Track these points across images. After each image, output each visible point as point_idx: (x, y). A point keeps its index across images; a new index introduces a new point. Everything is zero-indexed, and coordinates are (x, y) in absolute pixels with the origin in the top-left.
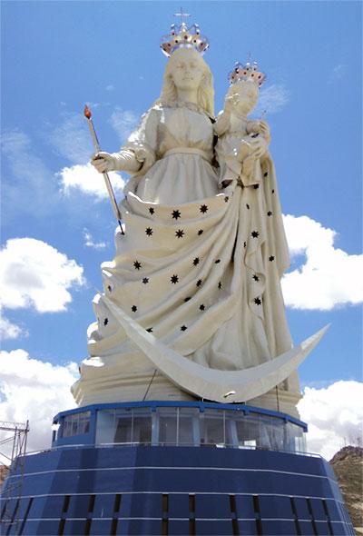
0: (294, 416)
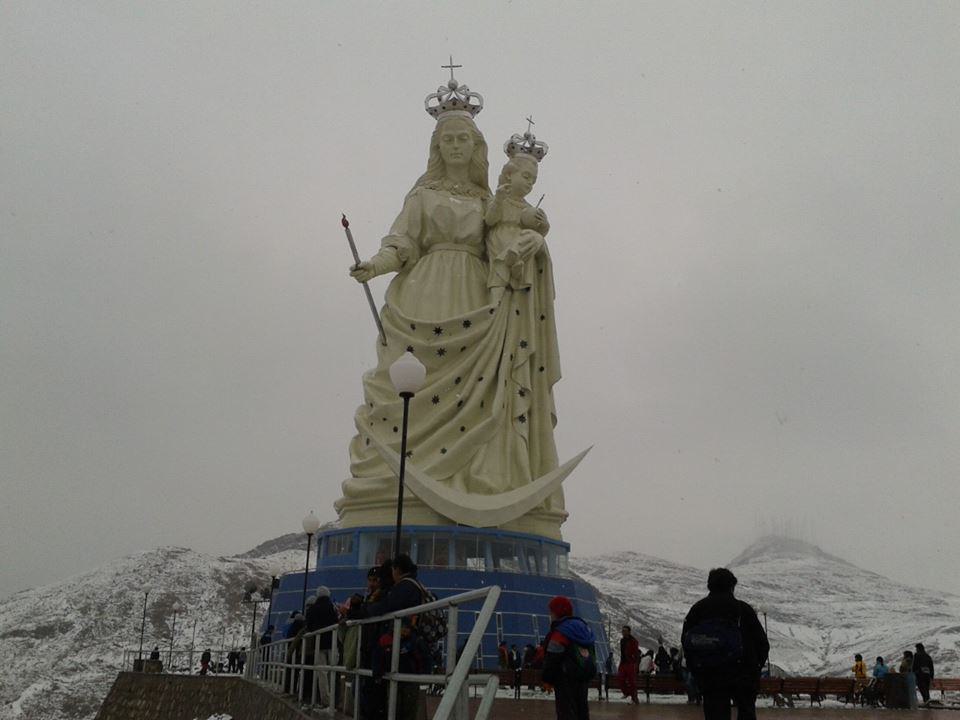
0: (557, 538)
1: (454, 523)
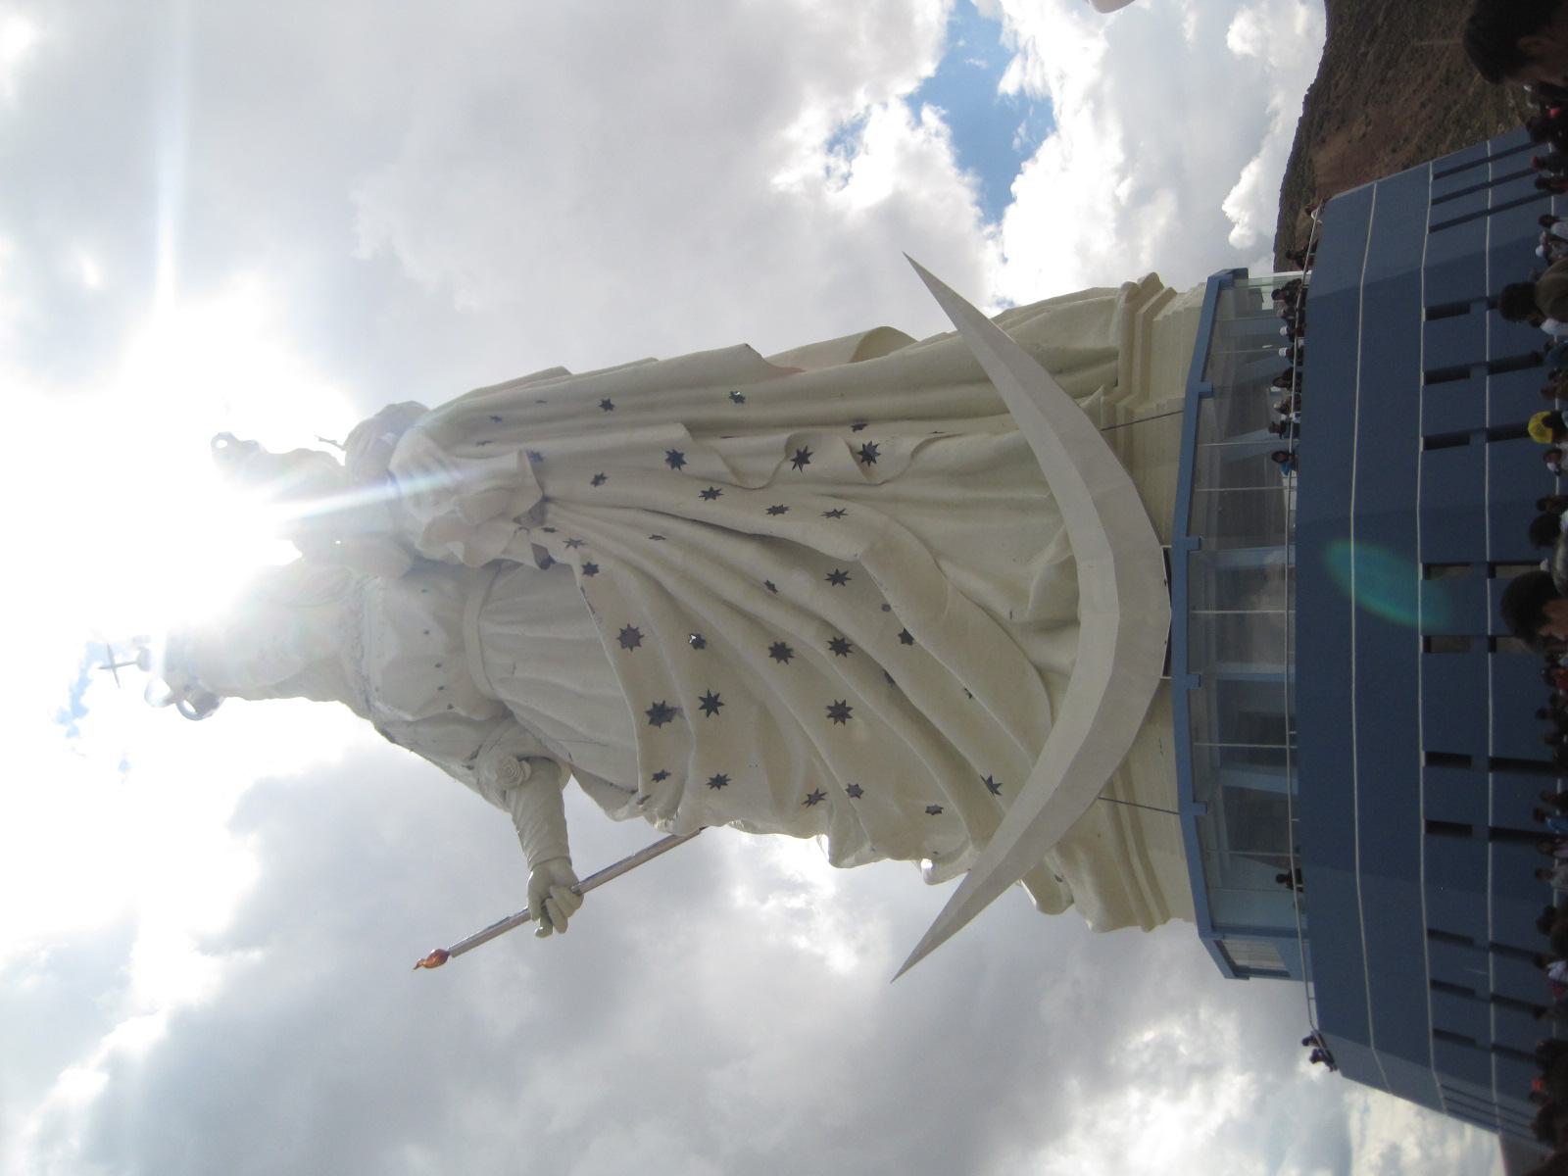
1: (1163, 683)
